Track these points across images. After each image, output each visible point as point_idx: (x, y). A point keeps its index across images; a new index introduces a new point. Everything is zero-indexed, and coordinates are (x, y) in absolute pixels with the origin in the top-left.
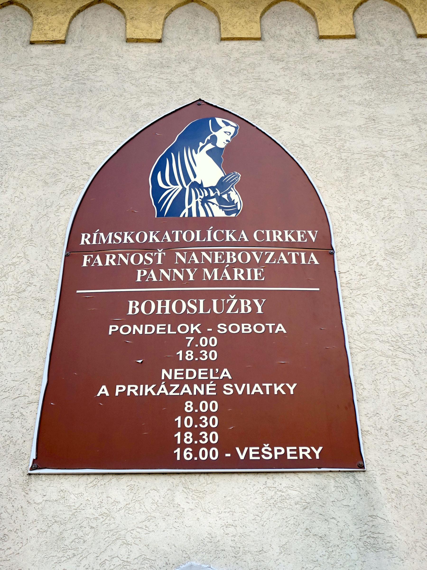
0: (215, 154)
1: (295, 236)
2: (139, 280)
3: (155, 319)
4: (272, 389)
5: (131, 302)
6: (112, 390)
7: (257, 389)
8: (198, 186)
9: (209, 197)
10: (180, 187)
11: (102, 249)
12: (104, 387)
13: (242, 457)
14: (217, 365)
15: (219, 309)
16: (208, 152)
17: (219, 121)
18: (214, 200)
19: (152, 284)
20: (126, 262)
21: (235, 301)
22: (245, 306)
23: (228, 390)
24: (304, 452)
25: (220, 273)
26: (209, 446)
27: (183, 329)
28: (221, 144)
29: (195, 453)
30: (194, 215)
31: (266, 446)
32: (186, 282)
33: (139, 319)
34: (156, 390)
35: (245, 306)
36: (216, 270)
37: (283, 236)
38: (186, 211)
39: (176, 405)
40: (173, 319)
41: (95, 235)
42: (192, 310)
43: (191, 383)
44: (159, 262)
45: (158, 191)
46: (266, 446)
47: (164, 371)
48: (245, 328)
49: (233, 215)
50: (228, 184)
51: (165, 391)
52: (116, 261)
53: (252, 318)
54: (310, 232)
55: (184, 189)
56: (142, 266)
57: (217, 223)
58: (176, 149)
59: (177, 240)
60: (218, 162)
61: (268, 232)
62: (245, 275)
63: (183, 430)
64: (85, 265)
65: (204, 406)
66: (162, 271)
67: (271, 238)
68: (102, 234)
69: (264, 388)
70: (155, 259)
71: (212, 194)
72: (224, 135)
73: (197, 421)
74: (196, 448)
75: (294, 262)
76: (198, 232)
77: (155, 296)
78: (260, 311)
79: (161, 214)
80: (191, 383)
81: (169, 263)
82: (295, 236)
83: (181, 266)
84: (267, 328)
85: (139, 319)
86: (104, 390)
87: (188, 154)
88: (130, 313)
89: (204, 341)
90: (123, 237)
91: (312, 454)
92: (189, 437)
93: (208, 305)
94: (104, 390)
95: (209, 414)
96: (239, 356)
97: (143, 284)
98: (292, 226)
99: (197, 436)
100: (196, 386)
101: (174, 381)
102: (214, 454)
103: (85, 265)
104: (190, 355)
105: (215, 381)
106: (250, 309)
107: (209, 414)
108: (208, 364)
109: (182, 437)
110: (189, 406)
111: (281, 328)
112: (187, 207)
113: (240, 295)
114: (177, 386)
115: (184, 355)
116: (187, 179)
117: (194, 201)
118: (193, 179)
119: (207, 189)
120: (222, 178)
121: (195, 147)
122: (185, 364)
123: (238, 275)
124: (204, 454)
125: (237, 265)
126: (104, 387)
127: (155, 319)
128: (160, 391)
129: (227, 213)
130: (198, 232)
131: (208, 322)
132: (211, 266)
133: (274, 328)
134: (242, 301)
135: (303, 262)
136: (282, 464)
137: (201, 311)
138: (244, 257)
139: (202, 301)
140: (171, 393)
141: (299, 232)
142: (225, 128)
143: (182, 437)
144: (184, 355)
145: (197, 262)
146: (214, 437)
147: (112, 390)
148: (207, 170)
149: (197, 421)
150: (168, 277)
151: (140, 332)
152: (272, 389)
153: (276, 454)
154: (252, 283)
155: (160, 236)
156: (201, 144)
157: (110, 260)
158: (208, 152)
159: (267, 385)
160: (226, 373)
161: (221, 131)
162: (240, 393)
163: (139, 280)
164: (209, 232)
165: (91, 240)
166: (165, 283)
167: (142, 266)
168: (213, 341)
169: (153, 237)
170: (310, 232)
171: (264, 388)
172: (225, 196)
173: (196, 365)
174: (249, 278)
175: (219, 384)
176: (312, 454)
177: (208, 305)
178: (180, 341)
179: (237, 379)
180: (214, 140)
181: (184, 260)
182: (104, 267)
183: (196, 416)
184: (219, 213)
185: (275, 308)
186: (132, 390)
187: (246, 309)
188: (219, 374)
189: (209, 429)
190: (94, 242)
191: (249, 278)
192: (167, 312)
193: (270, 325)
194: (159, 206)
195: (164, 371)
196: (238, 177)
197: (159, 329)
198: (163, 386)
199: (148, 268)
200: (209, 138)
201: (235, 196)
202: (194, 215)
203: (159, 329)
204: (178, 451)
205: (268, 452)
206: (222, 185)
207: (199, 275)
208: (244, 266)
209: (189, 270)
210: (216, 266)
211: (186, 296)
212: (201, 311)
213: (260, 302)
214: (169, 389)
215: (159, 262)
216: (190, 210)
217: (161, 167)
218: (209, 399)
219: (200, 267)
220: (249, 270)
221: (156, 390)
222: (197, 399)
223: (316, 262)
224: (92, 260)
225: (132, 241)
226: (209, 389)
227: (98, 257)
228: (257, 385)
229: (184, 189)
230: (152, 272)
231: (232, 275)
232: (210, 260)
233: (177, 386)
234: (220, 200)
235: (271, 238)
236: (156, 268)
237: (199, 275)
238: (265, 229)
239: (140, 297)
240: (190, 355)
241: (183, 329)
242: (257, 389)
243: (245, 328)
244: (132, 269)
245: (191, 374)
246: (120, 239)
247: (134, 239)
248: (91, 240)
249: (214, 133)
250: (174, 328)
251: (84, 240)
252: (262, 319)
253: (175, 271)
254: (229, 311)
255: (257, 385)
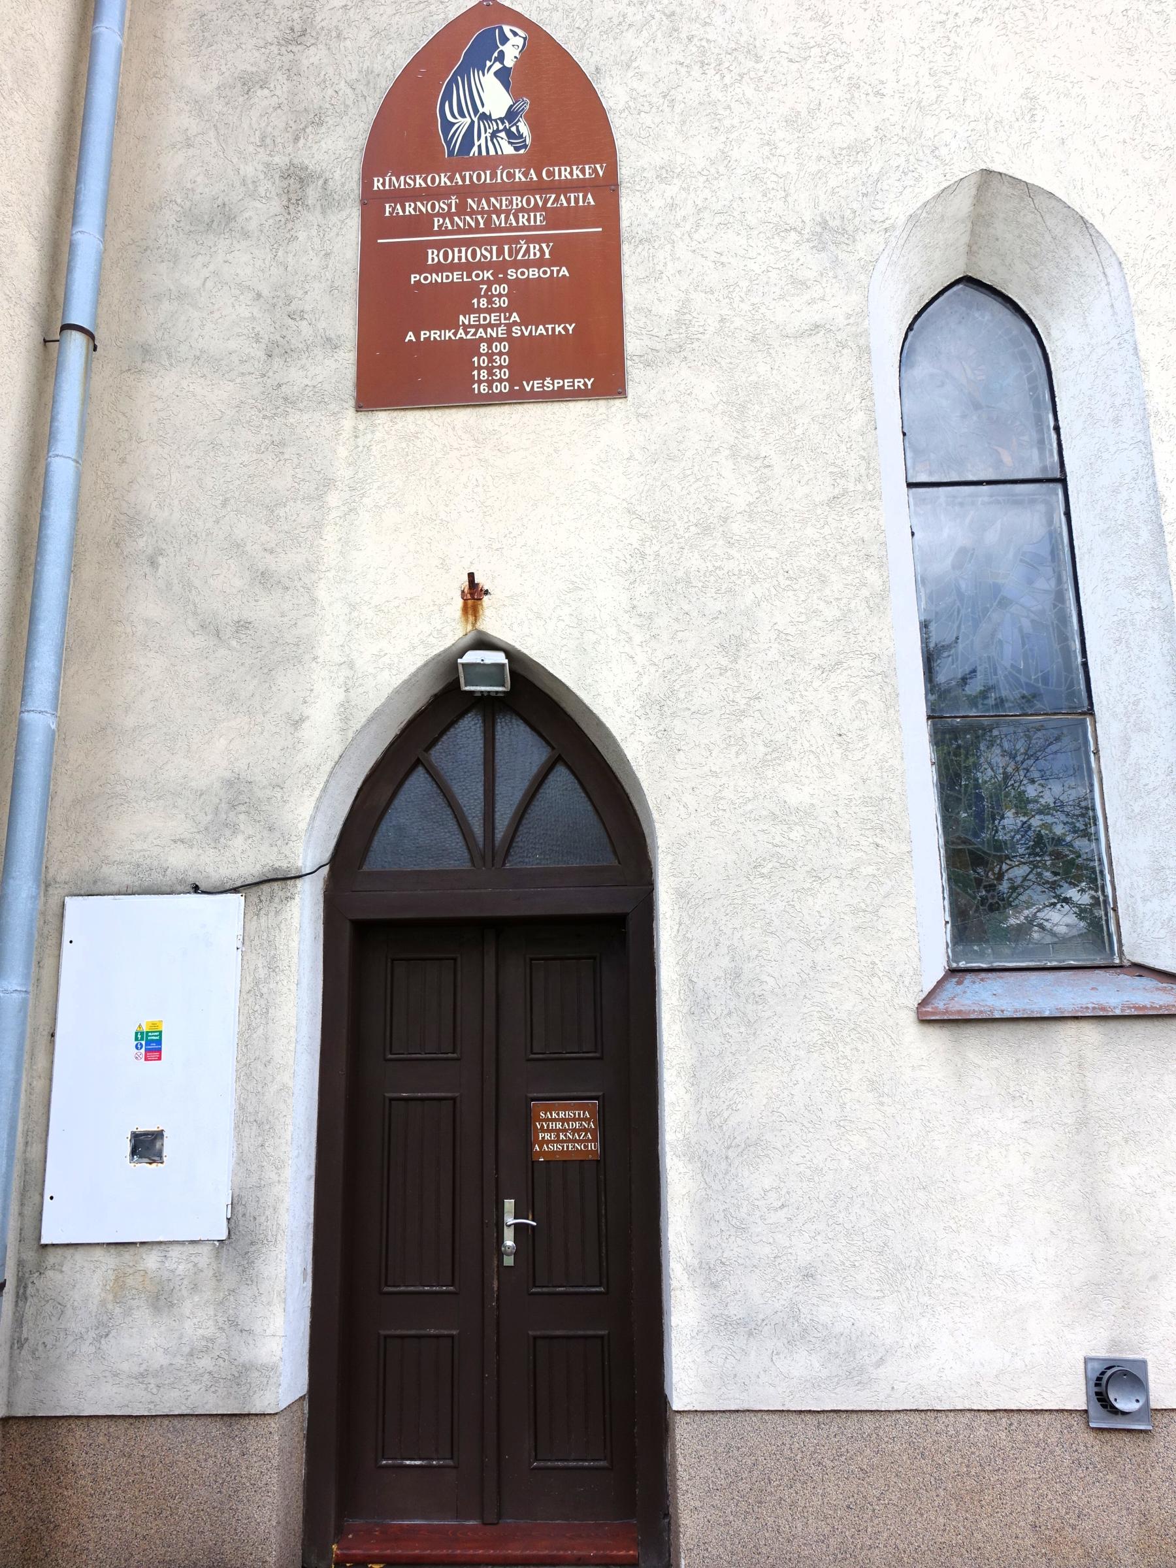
0: (503, 76)
1: (583, 171)
2: (436, 228)
3: (452, 268)
4: (553, 329)
5: (430, 251)
6: (417, 336)
7: (541, 330)
8: (485, 117)
9: (498, 131)
10: (468, 121)
11: (401, 196)
12: (410, 333)
13: (528, 389)
14: (510, 310)
15: (510, 256)
16: (496, 74)
17: (507, 29)
18: (503, 134)
19: (447, 232)
20: (424, 210)
21: (525, 247)
22: (534, 251)
23: (516, 332)
24: (579, 383)
25: (507, 219)
26: (501, 381)
27: (477, 276)
28: (509, 62)
29: (490, 387)
30: (484, 153)
31: (548, 380)
32: (477, 230)
33: (438, 268)
34: (455, 334)
35: (534, 251)
36: (503, 216)
37: (571, 173)
38: (475, 149)
39: (472, 347)
40: (468, 267)
41: (387, 179)
42: (486, 257)
43: (485, 327)
44: (453, 210)
45: (448, 125)
46: (548, 380)
47: (461, 317)
48: (533, 273)
49: (522, 151)
50: (517, 114)
51: (463, 335)
52: (415, 209)
53: (539, 263)
54: (598, 166)
55: (473, 122)
56: (438, 215)
57: (507, 161)
58: (464, 71)
59: (468, 182)
60: (506, 85)
61: (557, 169)
62: (529, 220)
63: (480, 368)
64: (387, 214)
65: (497, 347)
66: (456, 219)
67: (560, 175)
68: (394, 178)
69: (547, 330)
70: (450, 206)
71: (501, 127)
72: (511, 52)
73: (491, 360)
74: (490, 383)
75: (573, 204)
76: (488, 172)
77: (451, 244)
78: (547, 256)
79: (451, 153)
80: (485, 327)
81: (462, 210)
82: (583, 171)
83: (472, 213)
84: (552, 272)
85: (438, 268)
86: (410, 336)
87: (475, 76)
88: (430, 262)
89: (496, 289)
90: (415, 181)
91: (585, 384)
92: (484, 373)
93: (500, 252)
94: (410, 336)
95: (500, 354)
96: (527, 301)
97: (440, 233)
98: (581, 161)
99: (490, 373)
100: (490, 327)
101: (470, 326)
102: (504, 388)
103: (387, 214)
104: (484, 303)
105: (505, 325)
106: (538, 255)
107: (500, 354)
108: (500, 310)
109: (479, 374)
110: (484, 347)
111: (564, 271)
112: (477, 143)
113: (530, 240)
114: (473, 330)
115: (479, 303)
116: (476, 110)
117: (483, 136)
118: (481, 110)
119: (495, 121)
120: (511, 106)
121: (482, 68)
122: (479, 311)
123: (523, 221)
124: (498, 388)
125: (522, 210)
126: (410, 333)
127: (452, 268)
128: (459, 336)
129: (517, 149)
130: (488, 172)
131: (500, 268)
132: (498, 212)
133: (558, 272)
134: (532, 246)
135: (581, 203)
136: (560, 396)
137: (494, 258)
138: (528, 202)
139: (494, 248)
140: (469, 337)
141: (587, 167)
142: (513, 41)
143: (479, 374)
144: (479, 303)
145: (486, 208)
146: (505, 374)
147: (417, 336)
148: (495, 98)
149: (491, 360)
150: (461, 225)
151: (439, 280)
152: (553, 329)
153: (556, 385)
154: (536, 228)
155: (451, 179)
156: (488, 64)
157: (409, 209)
158: (496, 74)
159: (550, 326)
160: (515, 317)
161: (509, 44)
162: (527, 334)
163: (436, 228)
164: (499, 172)
165: (384, 184)
166: (459, 231)
167: (438, 215)
168: (504, 289)
169: (443, 180)
170: (598, 166)
171: (547, 330)
172: (514, 129)
173: (489, 311)
174: (532, 223)
175: (509, 327)
176: (585, 384)
177: (500, 252)
178: (472, 289)
179: (525, 322)
180: (501, 57)
181: (475, 207)
182: (404, 216)
183: (490, 356)
184: (508, 150)
185: (562, 252)
186: (435, 335)
187: (535, 254)
188: (509, 318)
189: (501, 367)
190: (387, 187)
191: (532, 223)
192: (463, 260)
193: (555, 269)
194: (448, 143)
195: (461, 317)
196: (526, 104)
197: (456, 277)
198: (461, 331)
199: (443, 216)
200: (496, 54)
201: (524, 129)
202: (484, 153)
203: (456, 277)
204: (476, 386)
205: (549, 384)
206: (511, 115)
207: (488, 221)
208: (528, 211)
209: (479, 217)
210: (502, 211)
211: (480, 243)
212: (494, 258)
213: (548, 246)
214: (467, 333)
215: (453, 210)
216: (480, 146)
217: (448, 96)
218: (500, 340)
219: (489, 213)
220: (532, 215)
221: (455, 334)
222: (490, 341)
223: (593, 203)
224: (394, 209)
225: (424, 185)
226: (501, 332)
227: (398, 206)
228: (541, 327)
229: (473, 122)
230: (447, 220)
231: (517, 221)
232: (498, 206)
233: (473, 330)
234: (510, 135)
235: (560, 175)
236: (450, 215)
237: (488, 221)
238: (553, 166)
239: (438, 245)
240: (484, 389)
241: (477, 276)
242: (541, 330)
243: (533, 273)
244: (429, 218)
245: (485, 319)
246: (412, 183)
247: (426, 182)
248: (384, 184)
249: (501, 48)
250: (469, 276)
251: (377, 184)
252: (550, 263)
253: (468, 218)
254: (519, 257)
255: (541, 327)
